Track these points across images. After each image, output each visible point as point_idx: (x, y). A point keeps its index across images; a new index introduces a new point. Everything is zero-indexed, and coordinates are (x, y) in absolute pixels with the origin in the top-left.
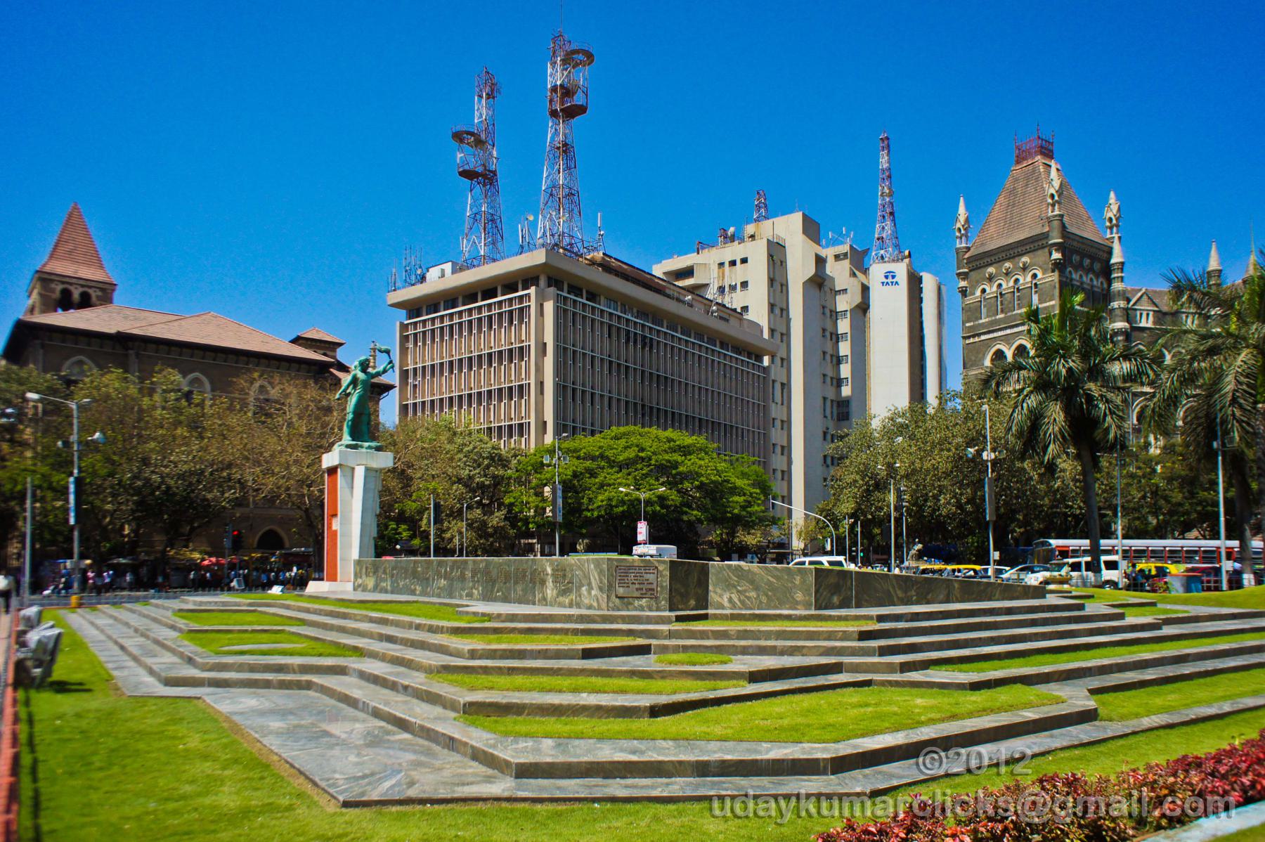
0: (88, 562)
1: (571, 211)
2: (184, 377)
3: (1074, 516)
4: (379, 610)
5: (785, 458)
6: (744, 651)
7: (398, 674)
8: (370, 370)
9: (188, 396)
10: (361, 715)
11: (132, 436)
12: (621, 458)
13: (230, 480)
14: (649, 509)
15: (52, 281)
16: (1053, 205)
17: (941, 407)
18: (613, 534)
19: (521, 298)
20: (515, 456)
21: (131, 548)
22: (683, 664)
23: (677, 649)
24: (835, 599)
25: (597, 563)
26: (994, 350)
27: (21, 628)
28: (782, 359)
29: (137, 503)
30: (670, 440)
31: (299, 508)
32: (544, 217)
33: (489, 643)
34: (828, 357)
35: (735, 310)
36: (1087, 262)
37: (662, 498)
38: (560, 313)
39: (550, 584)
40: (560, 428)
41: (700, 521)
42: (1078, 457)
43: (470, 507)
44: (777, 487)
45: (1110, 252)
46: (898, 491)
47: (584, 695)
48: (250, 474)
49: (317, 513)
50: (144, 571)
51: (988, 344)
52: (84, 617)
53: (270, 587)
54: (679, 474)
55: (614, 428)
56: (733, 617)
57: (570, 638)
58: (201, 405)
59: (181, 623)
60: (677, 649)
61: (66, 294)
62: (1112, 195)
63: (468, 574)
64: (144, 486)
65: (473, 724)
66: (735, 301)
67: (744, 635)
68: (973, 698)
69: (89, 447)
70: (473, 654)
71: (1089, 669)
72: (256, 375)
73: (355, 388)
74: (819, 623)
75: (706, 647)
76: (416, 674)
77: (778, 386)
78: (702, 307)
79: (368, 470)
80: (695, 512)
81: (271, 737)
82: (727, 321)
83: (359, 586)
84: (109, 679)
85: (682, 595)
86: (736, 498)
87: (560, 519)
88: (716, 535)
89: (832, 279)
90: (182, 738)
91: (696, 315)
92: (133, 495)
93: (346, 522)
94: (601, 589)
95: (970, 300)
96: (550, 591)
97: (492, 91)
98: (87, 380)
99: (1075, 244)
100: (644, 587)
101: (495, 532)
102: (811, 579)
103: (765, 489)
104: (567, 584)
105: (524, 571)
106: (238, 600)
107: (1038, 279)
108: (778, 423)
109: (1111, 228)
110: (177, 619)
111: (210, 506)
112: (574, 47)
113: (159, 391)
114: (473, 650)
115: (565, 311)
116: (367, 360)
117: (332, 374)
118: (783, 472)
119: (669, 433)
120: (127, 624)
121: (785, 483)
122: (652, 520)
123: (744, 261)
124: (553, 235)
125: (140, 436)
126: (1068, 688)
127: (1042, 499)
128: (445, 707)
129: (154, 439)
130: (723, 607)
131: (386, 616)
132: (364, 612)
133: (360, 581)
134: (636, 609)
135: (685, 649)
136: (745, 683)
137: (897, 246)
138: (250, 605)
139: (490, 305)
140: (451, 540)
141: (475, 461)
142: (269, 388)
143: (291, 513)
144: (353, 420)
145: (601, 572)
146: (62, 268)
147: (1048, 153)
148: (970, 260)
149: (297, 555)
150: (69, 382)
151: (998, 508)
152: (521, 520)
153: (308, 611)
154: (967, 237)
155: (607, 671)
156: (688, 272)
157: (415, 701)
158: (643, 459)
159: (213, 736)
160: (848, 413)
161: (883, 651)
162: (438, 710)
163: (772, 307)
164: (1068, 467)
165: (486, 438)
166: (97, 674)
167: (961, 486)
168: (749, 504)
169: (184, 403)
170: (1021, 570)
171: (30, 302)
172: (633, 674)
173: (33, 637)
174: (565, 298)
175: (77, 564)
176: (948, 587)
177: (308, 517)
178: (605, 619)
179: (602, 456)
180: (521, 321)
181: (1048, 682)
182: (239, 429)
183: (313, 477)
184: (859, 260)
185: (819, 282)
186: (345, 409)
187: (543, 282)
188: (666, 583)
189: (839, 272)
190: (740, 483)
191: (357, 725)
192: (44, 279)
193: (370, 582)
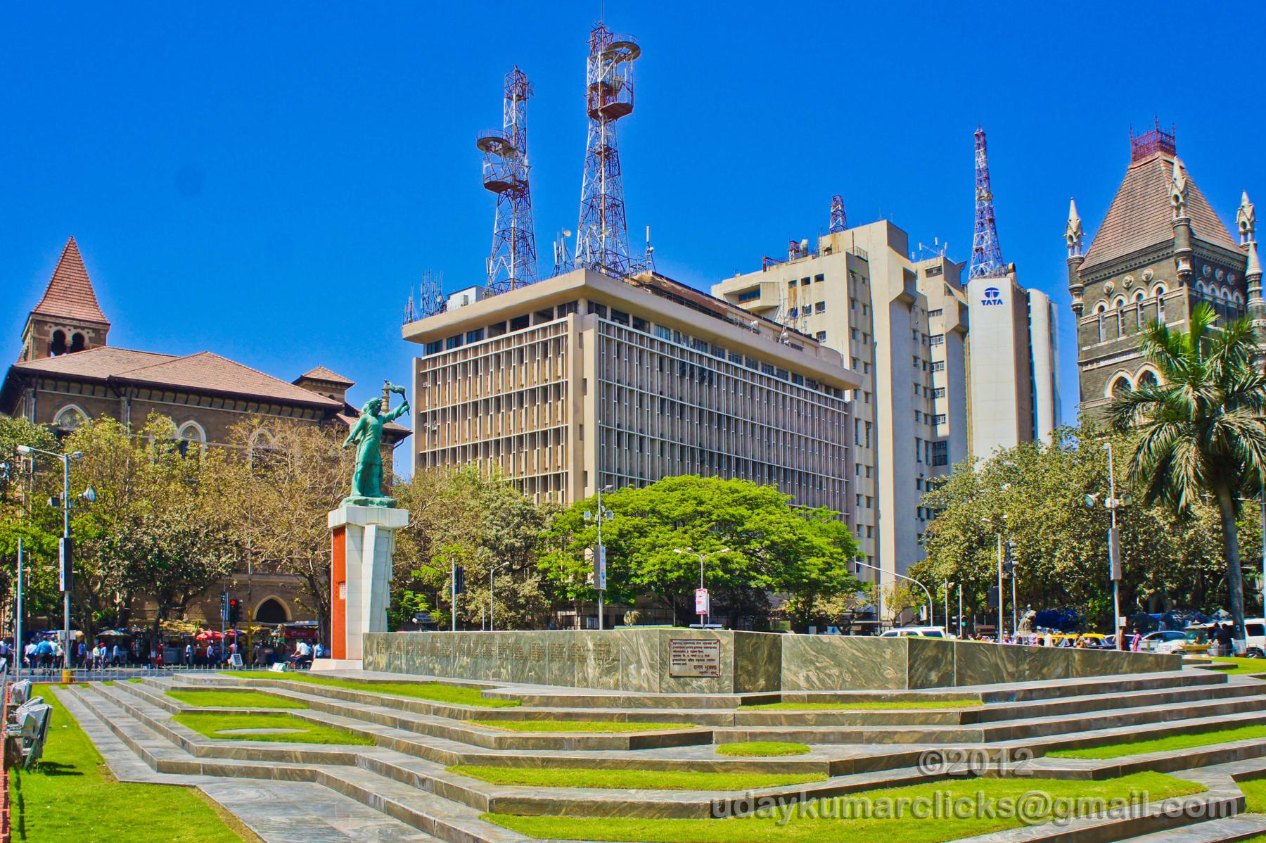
0: (80, 633)
1: (615, 224)
2: (178, 426)
3: (1212, 573)
4: (393, 692)
5: (871, 511)
6: (825, 739)
7: (414, 765)
8: (382, 414)
9: (183, 446)
10: (372, 811)
11: (123, 493)
12: (676, 513)
13: (226, 542)
14: (710, 574)
15: (46, 323)
16: (1178, 208)
17: (1056, 448)
18: (668, 602)
19: (557, 326)
20: (551, 513)
21: (122, 619)
22: (751, 754)
23: (743, 737)
24: (934, 676)
25: (648, 638)
26: (1120, 374)
27: (12, 703)
28: (867, 394)
29: (129, 568)
30: (733, 491)
31: (303, 574)
32: (583, 232)
33: (521, 730)
34: (921, 391)
35: (809, 337)
36: (1219, 274)
37: (725, 561)
38: (603, 344)
39: (591, 662)
40: (605, 479)
41: (770, 588)
42: (1216, 502)
43: (497, 574)
44: (863, 546)
45: (1245, 262)
46: (1007, 547)
47: (633, 791)
48: (247, 535)
49: (322, 580)
50: (136, 645)
51: (1107, 371)
52: (75, 694)
53: (271, 664)
54: (746, 531)
55: (667, 478)
56: (811, 699)
57: (616, 724)
58: (196, 457)
59: (174, 702)
60: (743, 737)
61: (60, 336)
62: (1245, 196)
63: (495, 650)
64: (135, 549)
65: (501, 824)
66: (810, 325)
67: (823, 719)
68: (1098, 789)
69: (82, 505)
70: (501, 743)
71: (1234, 751)
72: (256, 422)
73: (364, 434)
74: (915, 705)
75: (779, 734)
76: (435, 765)
77: (862, 426)
78: (771, 333)
79: (379, 529)
80: (765, 577)
81: (271, 832)
82: (800, 348)
83: (370, 664)
84: (100, 763)
85: (749, 674)
86: (813, 560)
87: (603, 586)
88: (787, 603)
89: (925, 298)
90: (176, 830)
91: (763, 343)
92: (124, 559)
93: (356, 590)
94: (652, 667)
95: (1086, 319)
96: (592, 669)
97: (524, 91)
98: (79, 431)
99: (1205, 252)
100: (704, 664)
101: (528, 603)
102: (904, 652)
103: (848, 549)
104: (611, 661)
105: (561, 646)
106: (235, 678)
107: (1167, 296)
108: (863, 470)
109: (1245, 234)
110: (171, 699)
111: (205, 572)
112: (616, 39)
113: (152, 441)
114: (501, 739)
115: (608, 340)
116: (379, 402)
117: (339, 419)
118: (869, 528)
119: (734, 483)
120: (118, 703)
121: (872, 541)
122: (714, 586)
123: (820, 278)
124: (593, 253)
125: (131, 493)
126: (1209, 775)
127: (1175, 553)
128: (468, 804)
129: (146, 496)
130: (799, 688)
131: (405, 699)
132: (375, 694)
133: (370, 658)
134: (694, 690)
135: (754, 737)
136: (826, 776)
137: (999, 259)
138: (249, 684)
139: (520, 336)
140: (475, 613)
141: (503, 519)
142: (269, 436)
143: (295, 580)
144: (363, 472)
145: (652, 647)
146: (56, 308)
147: (1169, 149)
148: (1085, 273)
149: (300, 628)
150: (60, 434)
151: (1123, 568)
152: (557, 588)
153: (312, 691)
154: (1080, 246)
155: (660, 763)
156: (754, 293)
157: (434, 796)
158: (702, 514)
159: (209, 829)
161: (990, 736)
162: (460, 807)
163: (853, 331)
164: (1205, 514)
165: (516, 492)
166: (87, 757)
167: (1079, 539)
168: (829, 567)
169: (178, 454)
170: (1152, 638)
171: (25, 347)
172: (690, 766)
173: (22, 713)
174: (608, 326)
175: (67, 636)
176: (1067, 658)
177: (313, 585)
178: (658, 702)
179: (653, 511)
180: (557, 353)
181: (1184, 768)
182: (236, 484)
183: (318, 539)
184: (956, 277)
185: (908, 301)
186: (353, 460)
187: (582, 307)
188: (730, 658)
189: (932, 290)
190: (819, 541)
191: (369, 823)
192: (39, 321)
193: (383, 660)
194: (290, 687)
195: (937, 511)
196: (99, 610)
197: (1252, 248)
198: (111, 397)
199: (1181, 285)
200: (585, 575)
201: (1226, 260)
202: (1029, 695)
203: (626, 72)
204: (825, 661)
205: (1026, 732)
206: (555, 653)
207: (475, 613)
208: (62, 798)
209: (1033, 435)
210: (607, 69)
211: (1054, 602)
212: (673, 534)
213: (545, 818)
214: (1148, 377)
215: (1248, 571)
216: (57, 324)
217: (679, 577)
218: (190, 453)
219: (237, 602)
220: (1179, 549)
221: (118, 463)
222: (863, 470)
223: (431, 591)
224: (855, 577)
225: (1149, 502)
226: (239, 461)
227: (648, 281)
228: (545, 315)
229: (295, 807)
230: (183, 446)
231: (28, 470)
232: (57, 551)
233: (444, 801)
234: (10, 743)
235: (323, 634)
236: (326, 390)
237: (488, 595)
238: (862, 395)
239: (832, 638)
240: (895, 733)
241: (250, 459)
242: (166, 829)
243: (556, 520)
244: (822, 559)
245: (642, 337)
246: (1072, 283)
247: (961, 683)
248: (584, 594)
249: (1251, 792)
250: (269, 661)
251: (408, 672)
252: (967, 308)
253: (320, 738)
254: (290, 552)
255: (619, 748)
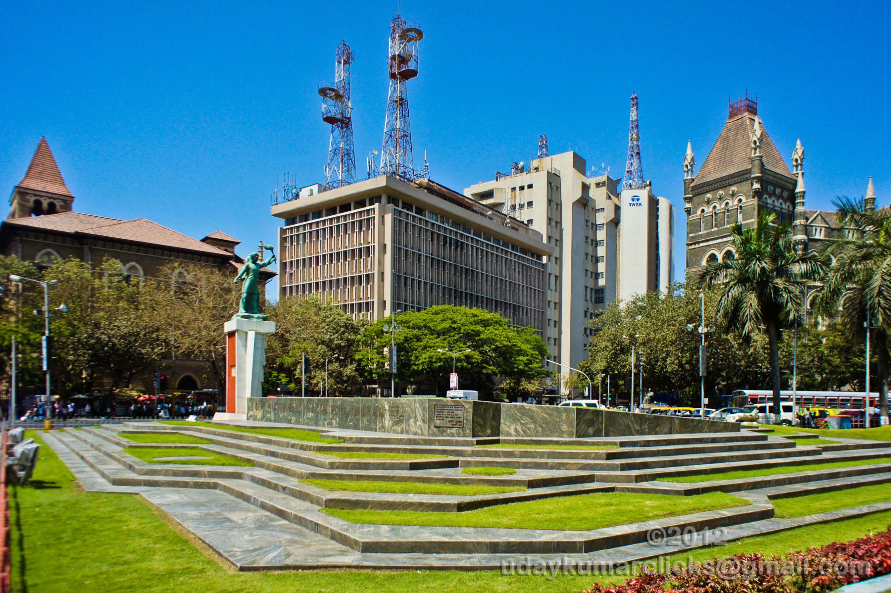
0: (57, 397)
1: (405, 148)
2: (124, 265)
3: (762, 373)
4: (266, 434)
5: (557, 329)
6: (525, 466)
7: (279, 479)
8: (258, 262)
9: (127, 279)
10: (253, 507)
11: (87, 308)
12: (439, 328)
13: (158, 340)
14: (459, 364)
15: (27, 194)
16: (755, 149)
17: (670, 295)
18: (433, 382)
19: (368, 211)
20: (363, 325)
21: (87, 388)
23: (477, 464)
24: (591, 430)
25: (421, 403)
27: (10, 443)
30: (474, 316)
31: (208, 360)
32: (385, 152)
33: (344, 458)
35: (523, 222)
36: (778, 191)
37: (468, 357)
38: (396, 222)
39: (387, 416)
40: (396, 306)
41: (495, 374)
42: (766, 332)
43: (330, 362)
44: (551, 350)
45: (795, 184)
47: (411, 495)
48: (172, 335)
50: (97, 403)
51: (704, 250)
54: (481, 340)
55: (434, 306)
56: (518, 442)
57: (401, 455)
58: (137, 285)
59: (124, 441)
60: (477, 464)
61: (38, 203)
62: (798, 142)
63: (329, 409)
64: (96, 343)
65: (332, 514)
66: (523, 216)
68: (687, 501)
69: (57, 315)
70: (332, 466)
71: (769, 481)
72: (176, 264)
73: (248, 275)
74: (578, 447)
76: (292, 479)
77: (553, 278)
78: (499, 220)
79: (257, 334)
80: (492, 367)
82: (517, 230)
84: (73, 480)
86: (521, 358)
87: (395, 371)
89: (594, 201)
90: (125, 521)
91: (494, 225)
92: (88, 350)
93: (242, 371)
94: (423, 421)
95: (693, 217)
96: (387, 422)
97: (348, 58)
98: (54, 266)
99: (770, 178)
103: (542, 352)
104: (399, 417)
105: (369, 408)
106: (164, 425)
107: (743, 204)
108: (552, 305)
109: (797, 166)
110: (122, 438)
112: (408, 27)
113: (106, 275)
115: (400, 221)
116: (257, 255)
117: (231, 264)
119: (475, 311)
120: (85, 441)
121: (557, 347)
122: (461, 372)
123: (530, 186)
125: (93, 307)
128: (312, 502)
129: (103, 310)
130: (510, 435)
131: (274, 438)
133: (251, 413)
134: (448, 435)
135: (483, 464)
136: (525, 488)
138: (173, 429)
139: (345, 216)
140: (317, 384)
141: (334, 329)
143: (203, 364)
144: (247, 298)
146: (35, 184)
148: (694, 188)
149: (207, 394)
150: (41, 268)
151: (708, 368)
152: (367, 371)
153: (214, 433)
154: (692, 171)
156: (489, 194)
157: (291, 498)
158: (455, 329)
159: (148, 520)
160: (603, 298)
161: (624, 467)
162: (307, 504)
163: (549, 220)
164: (759, 339)
165: (342, 312)
166: (65, 476)
168: (530, 362)
169: (124, 284)
170: (724, 411)
172: (446, 481)
173: (18, 449)
174: (400, 212)
175: (49, 398)
176: (671, 422)
177: (214, 367)
178: (426, 442)
179: (425, 327)
180: (368, 228)
181: (739, 490)
182: (165, 303)
183: (218, 339)
184: (613, 187)
185: (584, 203)
186: (240, 290)
187: (384, 199)
188: (470, 417)
189: (599, 196)
190: (524, 347)
191: (250, 514)
193: (259, 414)
194: (200, 431)
195: (596, 331)
196: (71, 382)
197: (800, 175)
198: (77, 246)
199: (754, 197)
200: (384, 364)
201: (784, 182)
202: (647, 443)
203: (413, 48)
204: (526, 420)
205: (645, 466)
206: (366, 411)
207: (317, 384)
208: (47, 503)
209: (656, 287)
210: (402, 46)
211: (668, 387)
212: (438, 340)
213: (358, 511)
214: (729, 254)
215: (785, 374)
216: (35, 195)
217: (440, 366)
218: (133, 283)
219: (165, 377)
220: (743, 358)
221: (83, 287)
222: (552, 305)
223: (289, 372)
224: (545, 369)
225: (727, 332)
226: (166, 289)
227: (425, 185)
228: (360, 203)
229: (204, 506)
230: (127, 279)
231: (18, 290)
232: (41, 344)
233: (297, 500)
234: (9, 470)
235: (218, 399)
236: (223, 246)
237: (325, 374)
238: (553, 259)
239: (530, 406)
240: (567, 464)
241: (173, 287)
242: (120, 521)
243: (366, 330)
244: (525, 358)
245: (420, 219)
246: (685, 194)
247: (607, 435)
248: (383, 375)
249: (778, 506)
250: (187, 415)
251: (275, 421)
252: (619, 208)
253: (220, 462)
254: (200, 347)
255: (403, 469)
